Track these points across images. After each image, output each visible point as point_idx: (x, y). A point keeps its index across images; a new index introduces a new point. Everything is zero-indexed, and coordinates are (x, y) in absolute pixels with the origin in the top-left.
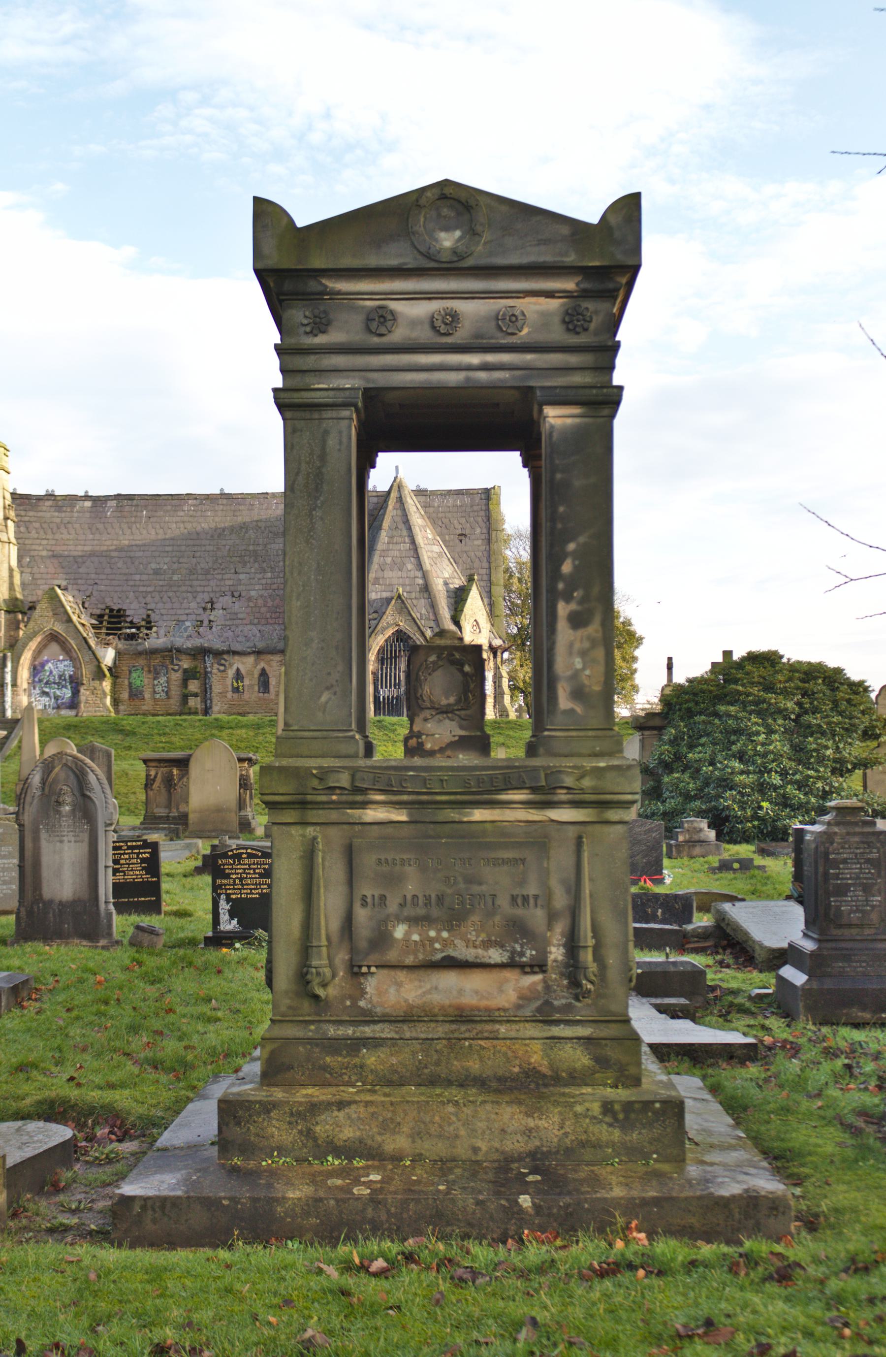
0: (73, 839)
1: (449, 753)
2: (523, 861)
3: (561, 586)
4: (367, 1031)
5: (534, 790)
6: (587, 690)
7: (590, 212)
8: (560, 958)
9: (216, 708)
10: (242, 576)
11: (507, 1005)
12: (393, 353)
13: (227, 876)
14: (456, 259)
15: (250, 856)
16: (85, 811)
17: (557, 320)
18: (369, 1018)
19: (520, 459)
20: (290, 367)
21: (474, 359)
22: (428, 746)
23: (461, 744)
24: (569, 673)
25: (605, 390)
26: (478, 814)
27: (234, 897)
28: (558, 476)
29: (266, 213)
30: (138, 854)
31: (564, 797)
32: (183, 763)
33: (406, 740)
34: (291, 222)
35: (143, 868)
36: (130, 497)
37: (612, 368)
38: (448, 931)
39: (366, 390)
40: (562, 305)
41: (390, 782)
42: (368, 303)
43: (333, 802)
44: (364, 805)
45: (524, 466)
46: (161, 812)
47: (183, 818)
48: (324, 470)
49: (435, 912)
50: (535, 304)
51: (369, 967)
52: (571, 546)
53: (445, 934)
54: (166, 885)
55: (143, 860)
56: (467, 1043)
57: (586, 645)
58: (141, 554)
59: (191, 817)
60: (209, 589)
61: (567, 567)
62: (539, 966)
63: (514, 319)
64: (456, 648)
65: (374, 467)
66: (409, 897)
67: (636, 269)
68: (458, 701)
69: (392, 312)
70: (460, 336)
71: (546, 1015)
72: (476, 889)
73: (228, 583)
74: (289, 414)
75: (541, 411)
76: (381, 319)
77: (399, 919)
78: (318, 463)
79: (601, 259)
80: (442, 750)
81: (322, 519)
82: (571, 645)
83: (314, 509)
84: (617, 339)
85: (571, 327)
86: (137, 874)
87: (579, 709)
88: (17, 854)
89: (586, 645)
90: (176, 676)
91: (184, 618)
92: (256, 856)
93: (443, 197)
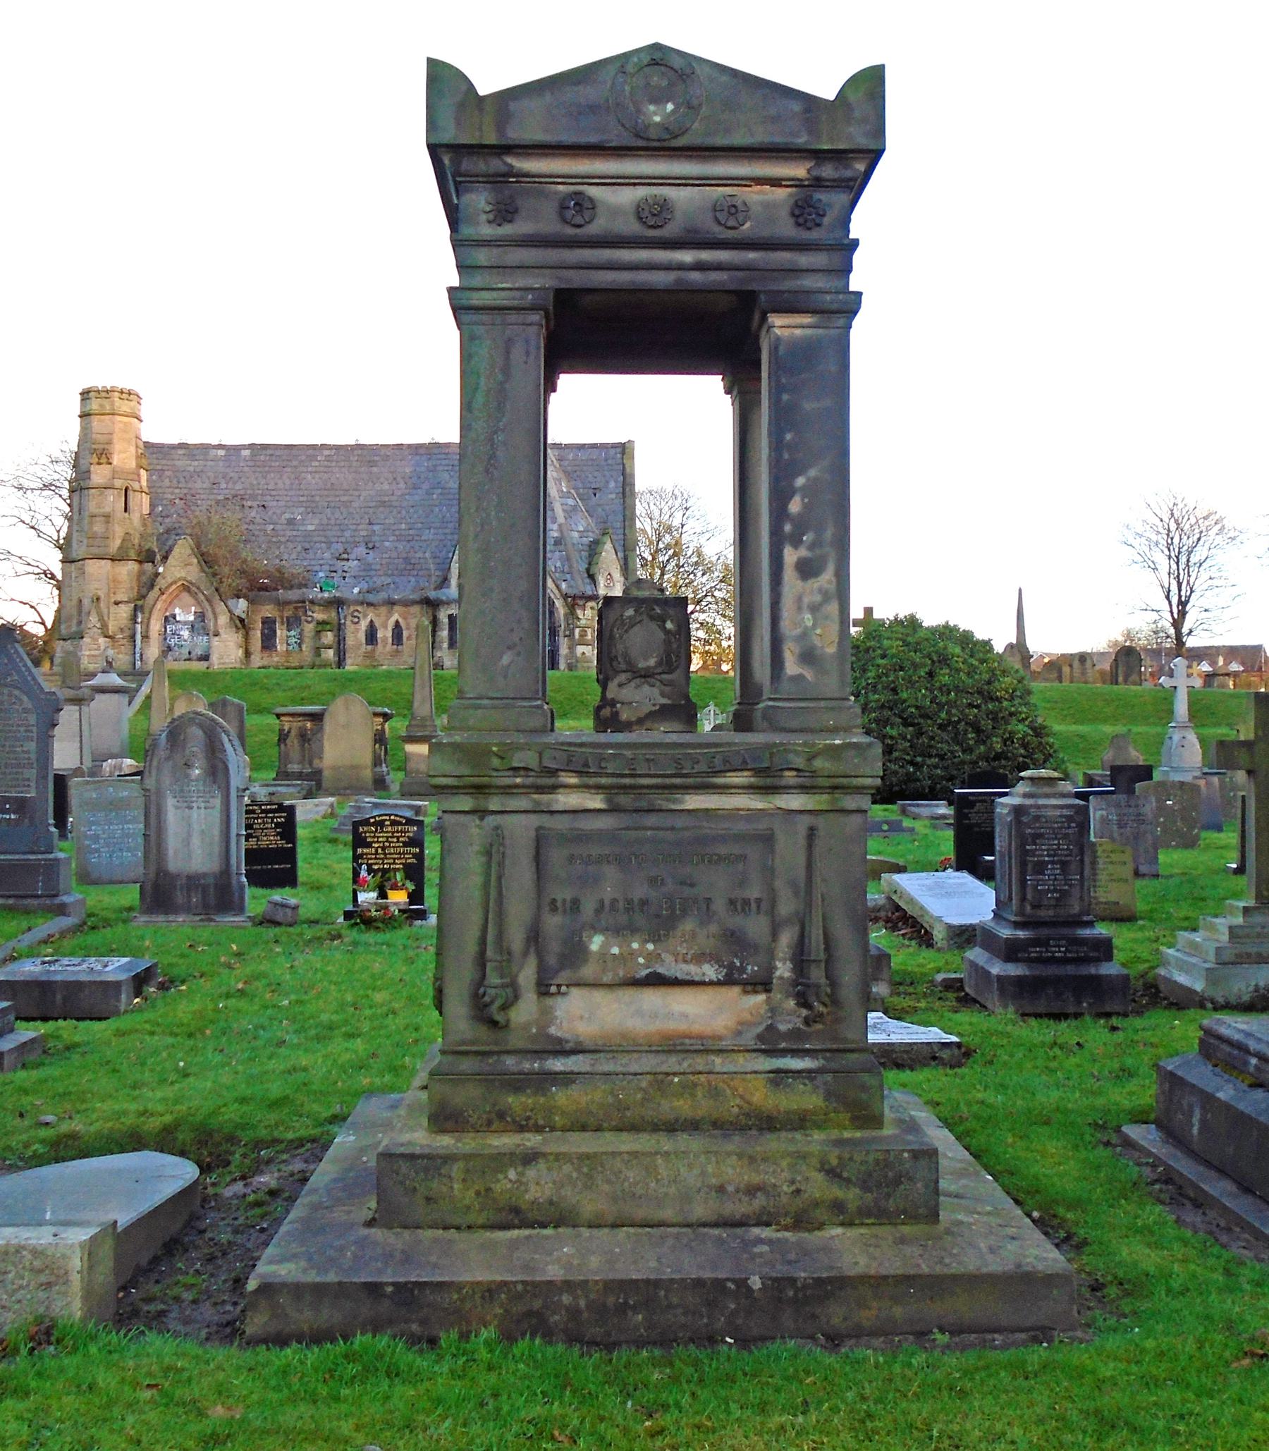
0: (203, 805)
1: (648, 724)
2: (743, 858)
3: (788, 528)
4: (557, 1065)
5: (758, 772)
6: (818, 652)
7: (825, 85)
8: (787, 974)
9: (349, 661)
10: (376, 528)
11: (723, 1032)
12: (591, 247)
13: (369, 845)
14: (668, 137)
15: (394, 823)
16: (217, 771)
17: (784, 213)
18: (561, 1049)
19: (722, 384)
20: (468, 262)
21: (687, 257)
22: (624, 716)
23: (663, 713)
24: (799, 631)
25: (841, 297)
26: (694, 801)
27: (376, 867)
28: (785, 397)
29: (441, 77)
30: (272, 818)
31: (792, 781)
32: (317, 717)
33: (598, 709)
34: (471, 86)
35: (278, 834)
36: (265, 447)
37: (849, 269)
38: (654, 942)
39: (559, 293)
40: (791, 195)
41: (582, 764)
42: (561, 187)
43: (517, 786)
44: (553, 789)
45: (727, 392)
46: (294, 767)
47: (316, 776)
48: (507, 386)
49: (640, 920)
50: (758, 193)
51: (559, 986)
52: (800, 481)
53: (650, 946)
54: (302, 853)
55: (278, 825)
56: (676, 1080)
57: (818, 598)
58: (275, 503)
59: (326, 773)
60: (343, 540)
61: (795, 506)
62: (762, 984)
63: (733, 210)
64: (657, 601)
65: (554, 391)
66: (607, 902)
67: (874, 155)
68: (659, 664)
69: (591, 199)
70: (668, 231)
71: (770, 1043)
72: (687, 891)
73: (362, 533)
74: (466, 318)
75: (764, 318)
76: (581, 205)
77: (595, 929)
78: (500, 377)
79: (836, 141)
80: (640, 721)
81: (505, 444)
82: (799, 599)
83: (495, 433)
84: (851, 236)
85: (801, 220)
86: (270, 840)
87: (809, 675)
88: (142, 819)
89: (818, 598)
90: (309, 628)
91: (317, 568)
92: (400, 823)
93: (654, 63)
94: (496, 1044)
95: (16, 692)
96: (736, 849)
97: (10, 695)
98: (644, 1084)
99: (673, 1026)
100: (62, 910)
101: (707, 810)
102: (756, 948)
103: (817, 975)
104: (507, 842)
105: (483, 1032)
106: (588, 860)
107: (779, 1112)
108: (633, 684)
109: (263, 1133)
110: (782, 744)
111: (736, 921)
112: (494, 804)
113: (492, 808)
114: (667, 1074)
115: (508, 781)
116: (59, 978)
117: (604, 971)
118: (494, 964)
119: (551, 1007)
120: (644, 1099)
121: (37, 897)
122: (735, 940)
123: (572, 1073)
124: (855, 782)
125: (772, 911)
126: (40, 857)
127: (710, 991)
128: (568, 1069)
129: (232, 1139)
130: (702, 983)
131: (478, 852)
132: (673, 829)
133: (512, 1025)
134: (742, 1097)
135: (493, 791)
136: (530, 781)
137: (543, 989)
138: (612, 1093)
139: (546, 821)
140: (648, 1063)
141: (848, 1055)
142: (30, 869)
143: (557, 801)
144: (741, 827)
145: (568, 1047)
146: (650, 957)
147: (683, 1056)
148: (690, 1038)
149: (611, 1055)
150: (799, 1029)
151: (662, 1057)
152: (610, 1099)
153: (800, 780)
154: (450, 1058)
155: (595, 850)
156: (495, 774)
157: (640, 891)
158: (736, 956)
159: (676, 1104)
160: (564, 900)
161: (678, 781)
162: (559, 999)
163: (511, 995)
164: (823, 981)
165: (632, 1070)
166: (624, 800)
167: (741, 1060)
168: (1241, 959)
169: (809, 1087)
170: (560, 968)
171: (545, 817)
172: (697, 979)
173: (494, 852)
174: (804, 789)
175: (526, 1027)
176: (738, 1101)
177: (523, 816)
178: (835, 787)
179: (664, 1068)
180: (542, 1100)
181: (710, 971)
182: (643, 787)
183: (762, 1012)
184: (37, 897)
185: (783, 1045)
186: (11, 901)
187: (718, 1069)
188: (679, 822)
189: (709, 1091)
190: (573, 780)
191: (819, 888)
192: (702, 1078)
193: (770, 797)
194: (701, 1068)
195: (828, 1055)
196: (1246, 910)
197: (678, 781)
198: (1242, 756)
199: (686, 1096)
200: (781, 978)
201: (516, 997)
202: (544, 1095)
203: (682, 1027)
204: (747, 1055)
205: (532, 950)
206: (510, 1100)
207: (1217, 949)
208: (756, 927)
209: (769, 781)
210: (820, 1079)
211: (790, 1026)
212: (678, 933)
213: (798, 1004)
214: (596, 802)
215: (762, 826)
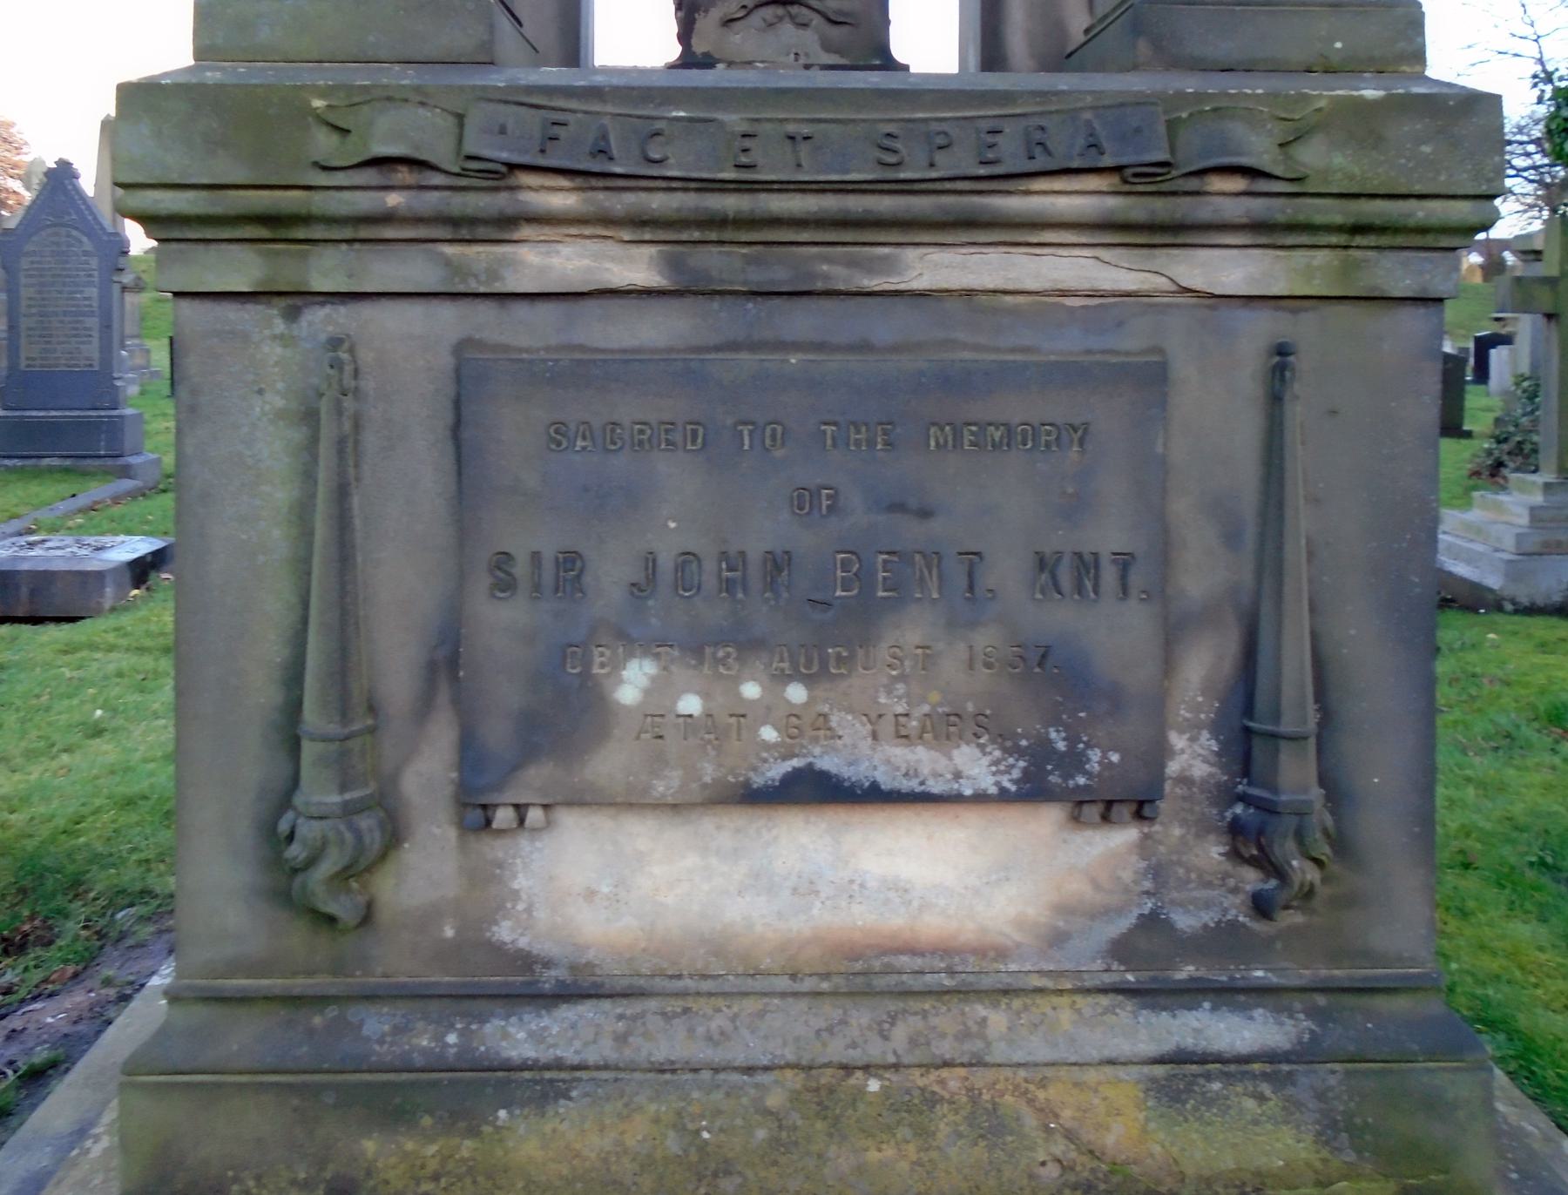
2: (1081, 433)
8: (1200, 770)
18: (534, 985)
31: (1236, 210)
38: (809, 680)
43: (388, 218)
44: (506, 225)
53: (797, 693)
56: (874, 1085)
62: (1133, 800)
66: (666, 562)
72: (912, 532)
77: (632, 642)
94: (338, 968)
95: (75, 233)
96: (1056, 408)
97: (69, 236)
98: (774, 1100)
99: (863, 918)
100: (126, 472)
101: (969, 293)
102: (1115, 699)
103: (1296, 777)
104: (368, 384)
105: (297, 938)
106: (609, 437)
107: (1182, 1176)
108: (757, 18)
109: (129, 876)
110: (1199, 97)
111: (1060, 618)
112: (326, 270)
113: (320, 284)
114: (848, 1069)
115: (363, 202)
116: (25, 566)
117: (658, 763)
118: (320, 746)
119: (500, 865)
120: (774, 1142)
121: (100, 457)
122: (1054, 674)
123: (558, 1065)
124: (1422, 212)
125: (1160, 593)
126: (103, 413)
127: (973, 817)
128: (546, 1055)
129: (76, 887)
130: (955, 799)
131: (280, 415)
132: (864, 347)
133: (384, 915)
134: (1070, 1135)
135: (318, 232)
136: (430, 201)
137: (476, 814)
138: (679, 1127)
139: (484, 321)
140: (785, 1031)
141: (1381, 1003)
142: (91, 427)
143: (514, 263)
144: (1068, 344)
145: (549, 979)
146: (796, 725)
147: (893, 1005)
148: (913, 951)
149: (676, 1005)
150: (1234, 925)
151: (830, 1011)
152: (673, 1144)
153: (1257, 207)
154: (200, 1012)
155: (628, 409)
156: (323, 179)
157: (765, 530)
158: (1056, 722)
159: (873, 1156)
160: (536, 557)
161: (885, 204)
162: (524, 842)
163: (374, 840)
164: (1316, 793)
165: (740, 1059)
166: (717, 262)
167: (1066, 1017)
168: (1551, 549)
169: (1274, 1104)
170: (527, 751)
171: (486, 310)
172: (936, 787)
173: (333, 422)
174: (1264, 232)
175: (428, 918)
176: (1059, 1147)
177: (415, 309)
178: (1358, 229)
179: (836, 1050)
180: (467, 1147)
181: (976, 766)
182: (775, 222)
183: (1127, 876)
184: (100, 457)
185: (1186, 971)
186: (68, 462)
187: (999, 1053)
188: (884, 326)
189: (971, 1120)
190: (561, 199)
191: (1302, 521)
192: (954, 1080)
193: (1161, 258)
194: (946, 1048)
195: (1321, 1000)
196: (1548, 487)
197: (885, 204)
198: (1545, 299)
199: (904, 1132)
200: (1184, 780)
201: (394, 836)
202: (473, 1132)
203: (895, 921)
204: (1081, 1001)
205: (443, 696)
206: (370, 1146)
207: (1518, 535)
208: (1114, 634)
209: (1161, 208)
210: (1308, 1079)
211: (1209, 918)
212: (883, 652)
213: (1235, 855)
214: (635, 266)
215: (1132, 341)
